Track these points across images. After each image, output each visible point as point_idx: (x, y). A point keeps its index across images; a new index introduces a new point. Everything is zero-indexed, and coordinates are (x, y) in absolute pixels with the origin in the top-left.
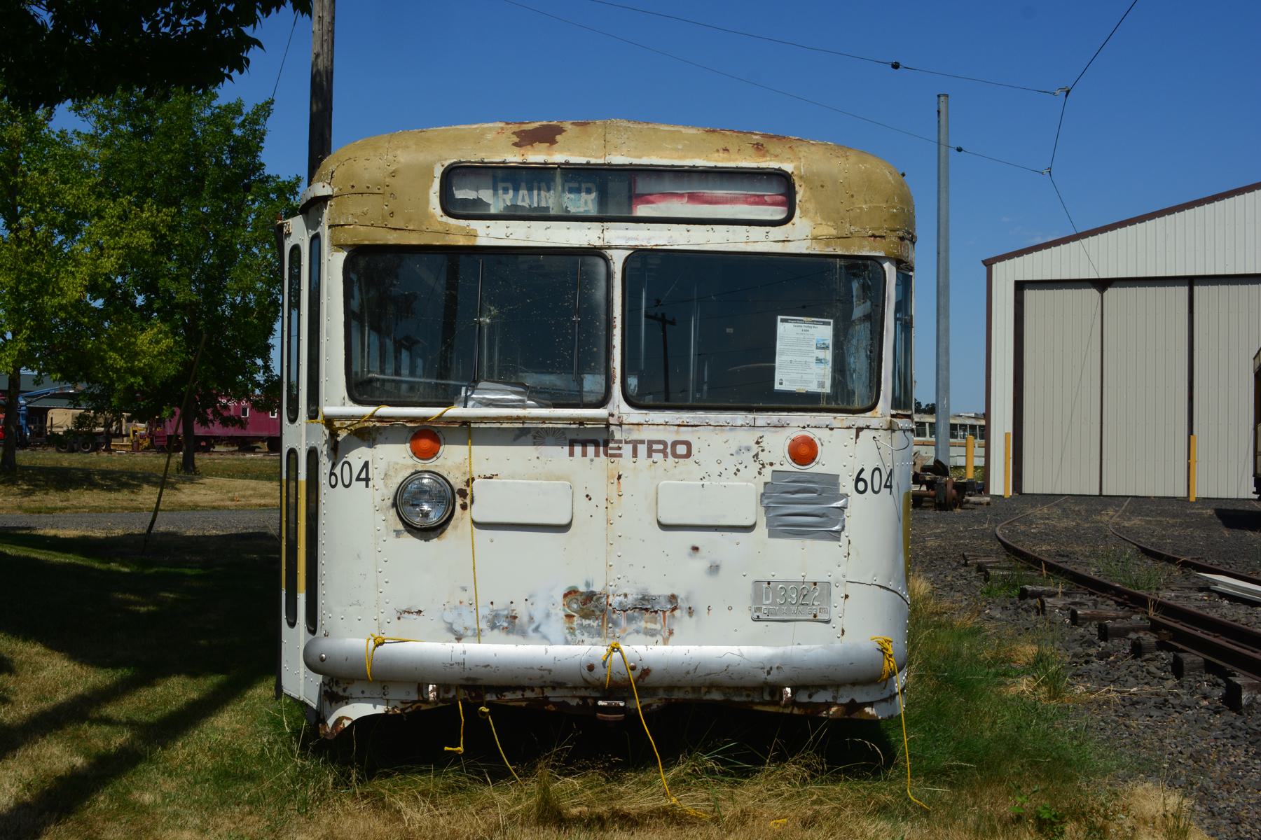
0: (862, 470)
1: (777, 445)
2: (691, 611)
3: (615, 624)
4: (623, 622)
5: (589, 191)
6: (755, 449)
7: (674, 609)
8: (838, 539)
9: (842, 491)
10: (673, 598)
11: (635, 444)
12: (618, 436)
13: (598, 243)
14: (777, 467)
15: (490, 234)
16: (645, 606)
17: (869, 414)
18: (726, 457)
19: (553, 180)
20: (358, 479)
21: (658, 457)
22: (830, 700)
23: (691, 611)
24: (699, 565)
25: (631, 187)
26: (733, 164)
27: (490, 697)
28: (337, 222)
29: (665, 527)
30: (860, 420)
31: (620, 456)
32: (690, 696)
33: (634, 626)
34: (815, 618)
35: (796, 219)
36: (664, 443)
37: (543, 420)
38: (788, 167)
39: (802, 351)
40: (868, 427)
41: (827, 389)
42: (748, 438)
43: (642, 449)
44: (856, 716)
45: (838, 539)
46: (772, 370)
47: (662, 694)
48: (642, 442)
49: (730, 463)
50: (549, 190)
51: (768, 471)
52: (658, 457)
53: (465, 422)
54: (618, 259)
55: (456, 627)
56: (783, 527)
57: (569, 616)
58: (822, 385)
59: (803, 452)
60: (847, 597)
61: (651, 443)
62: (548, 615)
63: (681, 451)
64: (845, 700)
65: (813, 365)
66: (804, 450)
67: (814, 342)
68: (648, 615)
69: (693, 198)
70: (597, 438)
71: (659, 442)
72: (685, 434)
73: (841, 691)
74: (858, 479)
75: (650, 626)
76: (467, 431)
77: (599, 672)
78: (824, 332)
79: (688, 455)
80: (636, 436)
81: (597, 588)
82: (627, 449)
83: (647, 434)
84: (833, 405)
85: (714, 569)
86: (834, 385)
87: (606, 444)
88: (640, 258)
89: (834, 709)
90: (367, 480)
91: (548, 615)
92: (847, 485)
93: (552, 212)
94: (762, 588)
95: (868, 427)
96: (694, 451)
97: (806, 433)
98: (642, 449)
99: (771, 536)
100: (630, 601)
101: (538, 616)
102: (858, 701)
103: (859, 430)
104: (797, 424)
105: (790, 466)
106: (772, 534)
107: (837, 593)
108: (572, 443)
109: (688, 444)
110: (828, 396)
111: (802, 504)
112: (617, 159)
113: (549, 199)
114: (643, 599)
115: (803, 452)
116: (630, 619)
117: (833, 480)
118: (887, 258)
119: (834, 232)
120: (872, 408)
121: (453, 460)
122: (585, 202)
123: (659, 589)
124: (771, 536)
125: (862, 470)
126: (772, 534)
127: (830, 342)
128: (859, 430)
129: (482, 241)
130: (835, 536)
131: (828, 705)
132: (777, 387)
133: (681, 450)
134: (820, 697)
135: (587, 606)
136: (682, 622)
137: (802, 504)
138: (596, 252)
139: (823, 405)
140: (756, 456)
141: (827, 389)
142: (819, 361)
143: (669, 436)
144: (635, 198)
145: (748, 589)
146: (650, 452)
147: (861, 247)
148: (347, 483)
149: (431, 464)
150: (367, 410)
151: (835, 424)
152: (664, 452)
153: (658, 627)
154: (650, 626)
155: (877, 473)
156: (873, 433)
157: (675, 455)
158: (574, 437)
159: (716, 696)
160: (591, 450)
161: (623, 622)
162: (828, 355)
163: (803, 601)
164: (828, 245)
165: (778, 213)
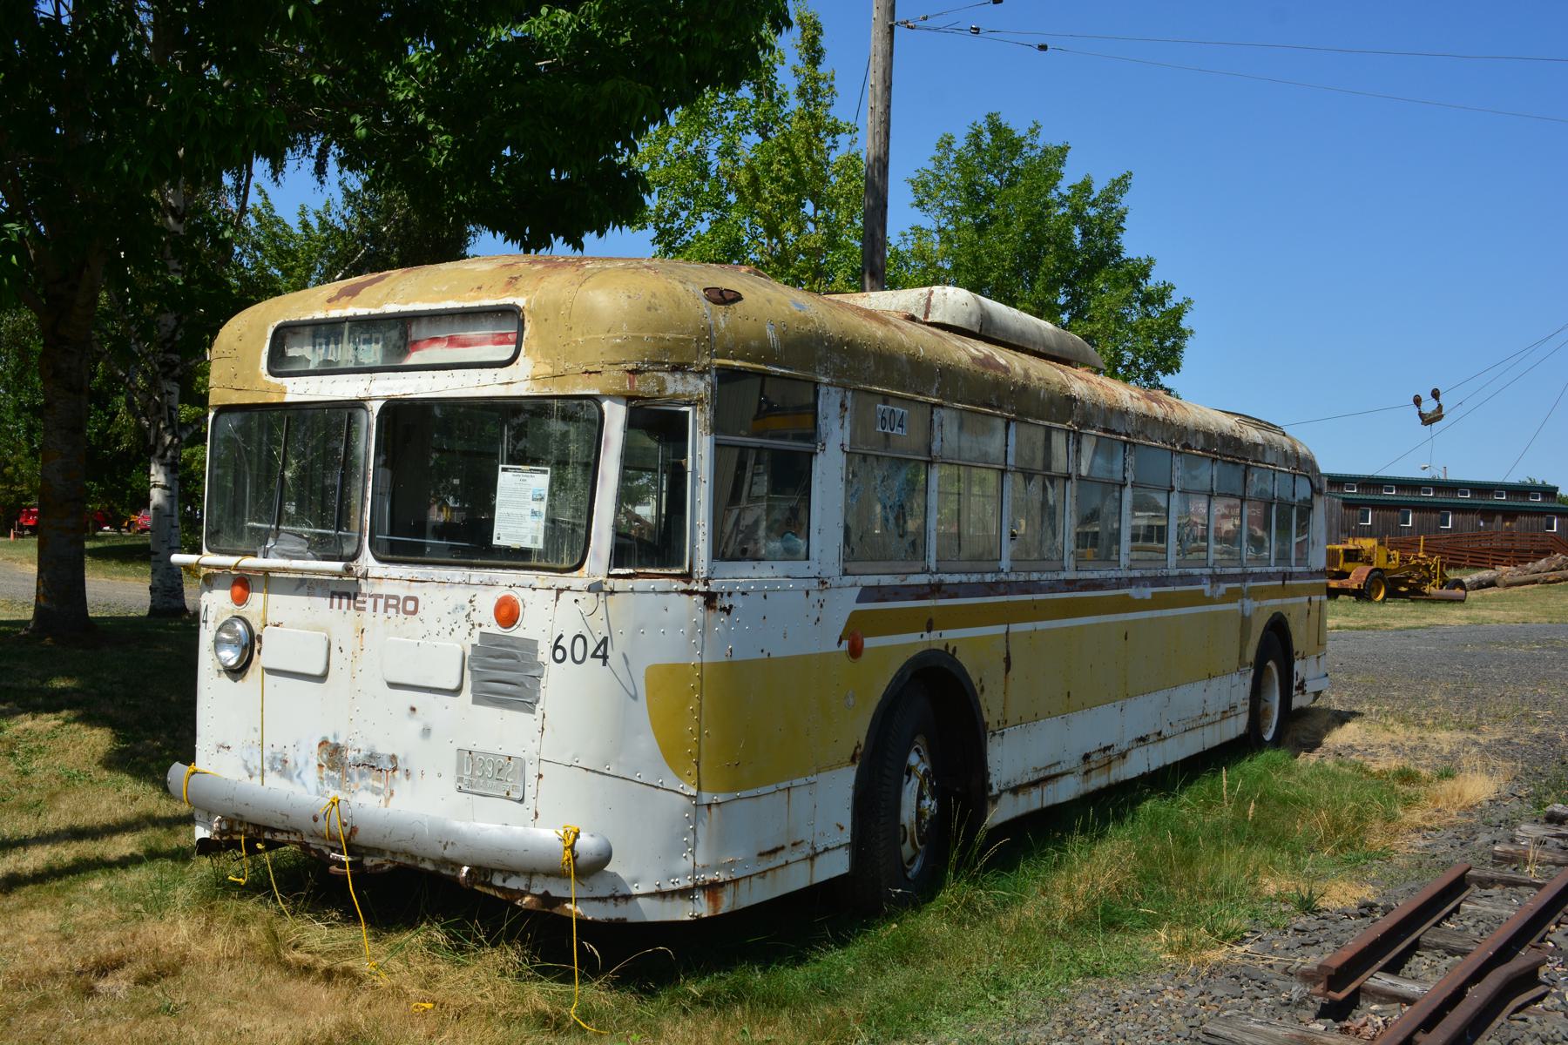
0: (561, 637)
1: (487, 602)
2: (408, 773)
3: (351, 779)
4: (356, 777)
5: (377, 342)
6: (468, 608)
7: (394, 770)
8: (533, 712)
9: (540, 658)
10: (393, 758)
11: (376, 597)
12: (364, 590)
13: (363, 395)
14: (485, 629)
15: (298, 390)
16: (371, 764)
17: (576, 574)
18: (435, 613)
19: (342, 334)
20: (594, 656)
21: (392, 611)
22: (523, 888)
23: (408, 773)
24: (415, 726)
25: (405, 335)
26: (476, 304)
27: (267, 836)
28: (1190, 487)
29: (393, 685)
30: (561, 581)
31: (363, 609)
32: (409, 862)
33: (363, 783)
34: (508, 796)
35: (520, 359)
36: (396, 597)
37: (315, 572)
38: (521, 302)
39: (520, 502)
40: (568, 589)
41: (540, 545)
42: (461, 595)
43: (381, 602)
44: (557, 910)
45: (533, 712)
46: (491, 522)
47: (388, 856)
48: (381, 596)
49: (447, 621)
50: (336, 344)
51: (476, 632)
52: (392, 611)
53: (266, 572)
54: (375, 407)
55: (251, 766)
56: (485, 696)
57: (320, 766)
58: (535, 540)
59: (508, 613)
60: (540, 776)
61: (388, 597)
62: (307, 763)
63: (408, 607)
64: (539, 891)
65: (529, 518)
66: (505, 612)
67: (530, 494)
68: (374, 773)
69: (452, 342)
70: (345, 591)
71: (394, 597)
72: (416, 590)
73: (535, 880)
74: (556, 647)
75: (376, 784)
76: (266, 581)
77: (322, 825)
78: (539, 481)
79: (415, 612)
80: (377, 590)
81: (341, 741)
82: (370, 601)
83: (385, 589)
84: (543, 564)
85: (426, 732)
86: (546, 541)
87: (356, 596)
88: (395, 410)
89: (527, 899)
90: (605, 657)
91: (307, 763)
92: (544, 653)
93: (342, 366)
94: (468, 757)
95: (568, 589)
96: (420, 608)
97: (935, 639)
98: (381, 602)
99: (475, 702)
100: (361, 757)
101: (301, 763)
102: (553, 894)
103: (560, 591)
104: (507, 580)
105: (496, 629)
106: (475, 701)
107: (530, 773)
108: (333, 594)
109: (416, 600)
110: (539, 553)
111: (502, 672)
112: (391, 308)
113: (343, 353)
114: (371, 756)
115: (508, 613)
116: (362, 776)
117: (531, 645)
118: (614, 397)
119: (550, 370)
120: (579, 567)
121: (256, 599)
122: (372, 353)
123: (384, 749)
124: (475, 702)
125: (561, 637)
126: (475, 701)
127: (546, 493)
128: (560, 591)
129: (289, 398)
130: (529, 707)
131: (522, 894)
132: (495, 542)
133: (410, 606)
134: (514, 883)
135: (333, 754)
136: (401, 785)
137: (502, 672)
138: (358, 404)
139: (534, 562)
140: (468, 615)
141: (540, 545)
142: (534, 513)
143: (401, 591)
144: (407, 345)
145: (453, 756)
146: (387, 606)
147: (575, 386)
148: (579, 657)
149: (242, 611)
150: (230, 561)
151: (537, 584)
152: (396, 607)
153: (382, 786)
154: (376, 784)
155: (579, 641)
156: (576, 596)
157: (406, 612)
158: (333, 588)
159: (429, 866)
160: (345, 601)
161: (356, 777)
162: (542, 507)
163: (487, 774)
164: (544, 385)
165: (505, 352)
